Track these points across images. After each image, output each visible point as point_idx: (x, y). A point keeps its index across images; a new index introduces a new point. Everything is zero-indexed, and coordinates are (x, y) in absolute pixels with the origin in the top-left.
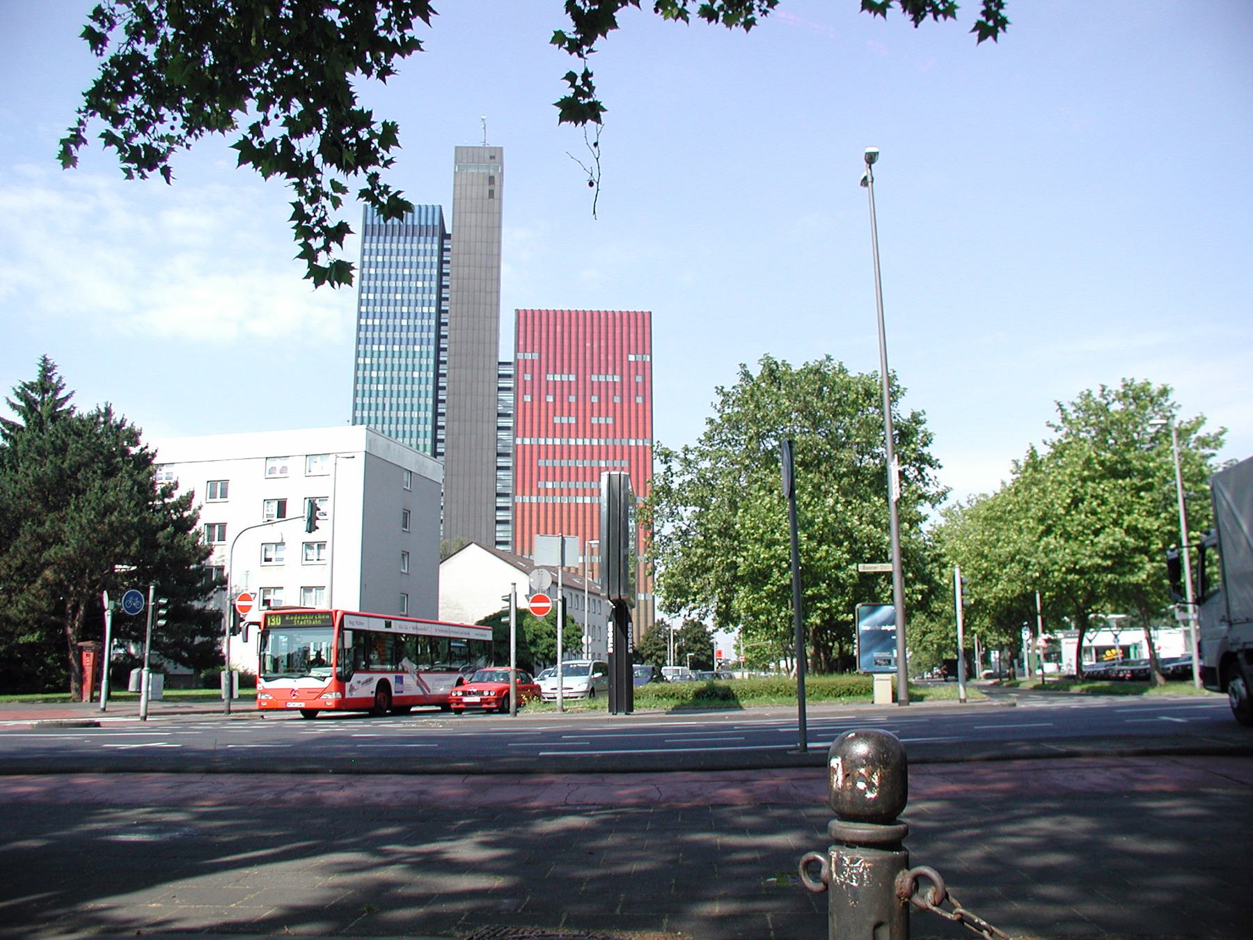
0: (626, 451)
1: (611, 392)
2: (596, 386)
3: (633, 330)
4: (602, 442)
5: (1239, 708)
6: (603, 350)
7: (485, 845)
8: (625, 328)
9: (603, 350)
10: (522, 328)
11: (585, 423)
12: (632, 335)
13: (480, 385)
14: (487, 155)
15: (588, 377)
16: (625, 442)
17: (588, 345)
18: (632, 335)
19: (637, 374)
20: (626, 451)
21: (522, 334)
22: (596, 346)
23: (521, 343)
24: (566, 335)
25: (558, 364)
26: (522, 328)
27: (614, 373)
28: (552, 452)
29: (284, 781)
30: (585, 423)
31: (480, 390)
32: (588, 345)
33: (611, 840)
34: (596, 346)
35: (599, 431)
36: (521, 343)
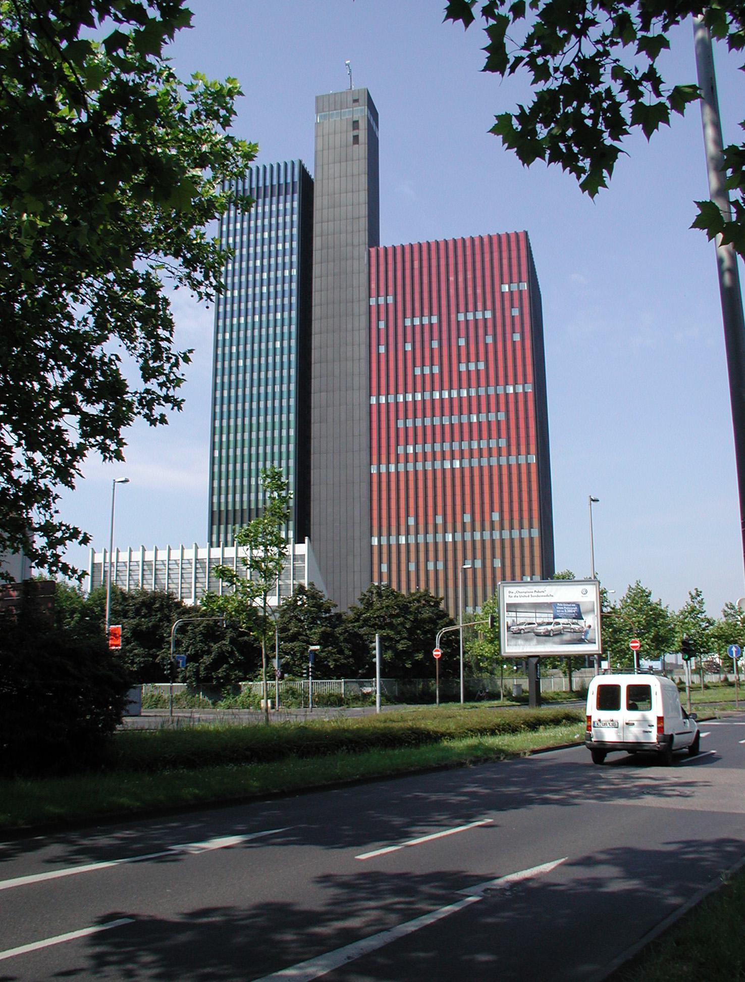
0: (502, 400)
1: (481, 331)
2: (463, 326)
3: (505, 255)
4: (473, 392)
5: (87, 266)
6: (470, 283)
7: (435, 887)
8: (496, 255)
9: (470, 283)
10: (374, 270)
11: (450, 371)
12: (505, 262)
13: (349, 348)
14: (350, 99)
15: (453, 316)
16: (500, 390)
17: (452, 279)
18: (505, 262)
19: (512, 307)
20: (502, 400)
21: (374, 277)
22: (461, 279)
23: (373, 286)
24: (425, 270)
25: (417, 305)
26: (374, 270)
27: (485, 309)
28: (407, 410)
29: (189, 792)
30: (450, 371)
31: (349, 354)
32: (452, 279)
33: (293, 945)
34: (461, 279)
35: (469, 380)
36: (373, 286)
